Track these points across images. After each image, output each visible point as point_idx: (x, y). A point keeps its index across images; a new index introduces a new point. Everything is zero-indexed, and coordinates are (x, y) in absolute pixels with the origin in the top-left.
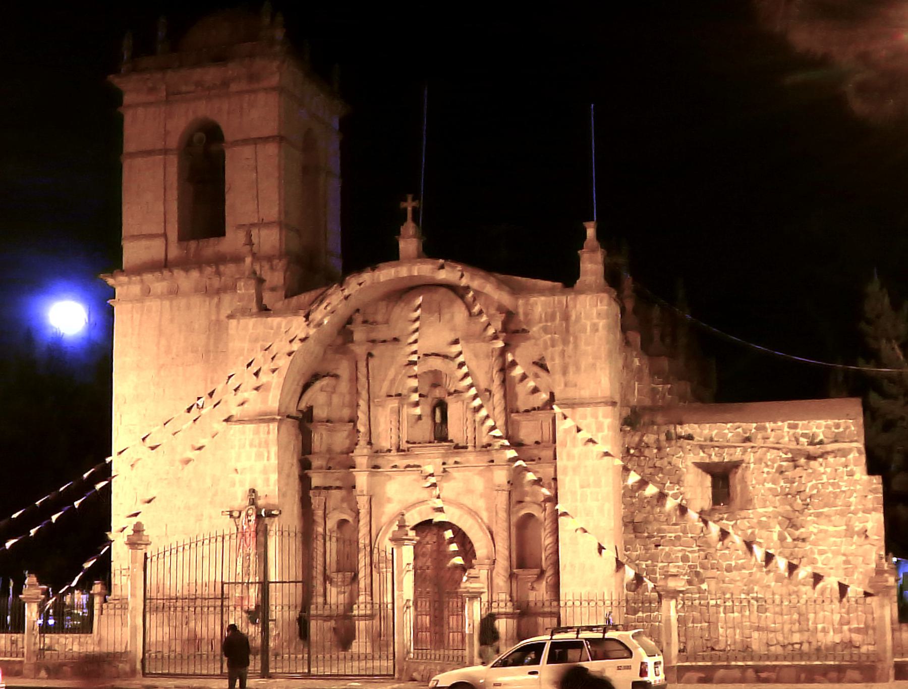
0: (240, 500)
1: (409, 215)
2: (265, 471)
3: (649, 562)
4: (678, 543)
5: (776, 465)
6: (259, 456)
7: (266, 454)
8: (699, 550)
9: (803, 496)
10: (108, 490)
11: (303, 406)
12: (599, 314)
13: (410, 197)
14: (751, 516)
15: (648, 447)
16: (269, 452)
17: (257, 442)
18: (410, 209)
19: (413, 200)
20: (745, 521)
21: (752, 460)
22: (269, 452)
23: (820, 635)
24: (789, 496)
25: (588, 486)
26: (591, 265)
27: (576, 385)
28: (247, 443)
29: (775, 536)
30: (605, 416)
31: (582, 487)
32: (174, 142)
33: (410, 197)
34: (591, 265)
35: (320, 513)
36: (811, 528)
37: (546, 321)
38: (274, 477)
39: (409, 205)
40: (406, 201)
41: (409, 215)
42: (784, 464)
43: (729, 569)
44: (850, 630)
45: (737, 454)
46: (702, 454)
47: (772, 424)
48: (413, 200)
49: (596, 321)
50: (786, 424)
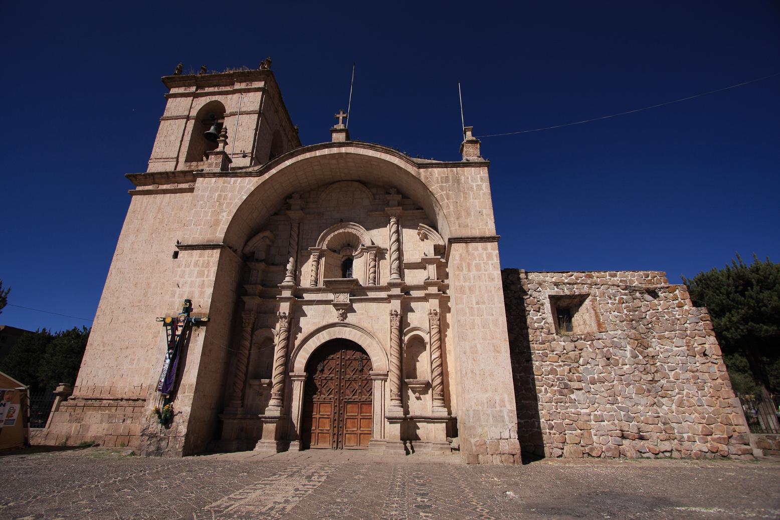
0: (177, 310)
1: (341, 121)
2: (202, 285)
3: (523, 374)
4: (545, 359)
5: (617, 298)
6: (201, 274)
7: (206, 273)
8: (565, 365)
9: (645, 322)
10: (169, 350)
11: (248, 249)
12: (482, 179)
13: (341, 113)
14: (604, 337)
15: (513, 283)
16: (208, 271)
17: (200, 263)
18: (341, 118)
19: (344, 113)
20: (600, 341)
21: (597, 294)
22: (208, 271)
23: (687, 444)
24: (634, 322)
25: (484, 303)
26: (471, 153)
27: (467, 226)
28: (192, 264)
29: (628, 354)
30: (493, 249)
31: (477, 303)
32: (194, 113)
33: (341, 113)
34: (471, 153)
35: (249, 330)
36: (655, 347)
37: (442, 183)
38: (210, 291)
39: (341, 116)
40: (339, 114)
41: (341, 121)
42: (624, 297)
43: (593, 382)
44: (713, 440)
45: (585, 289)
46: (556, 289)
47: (596, 274)
48: (344, 113)
49: (480, 183)
50: (607, 273)
